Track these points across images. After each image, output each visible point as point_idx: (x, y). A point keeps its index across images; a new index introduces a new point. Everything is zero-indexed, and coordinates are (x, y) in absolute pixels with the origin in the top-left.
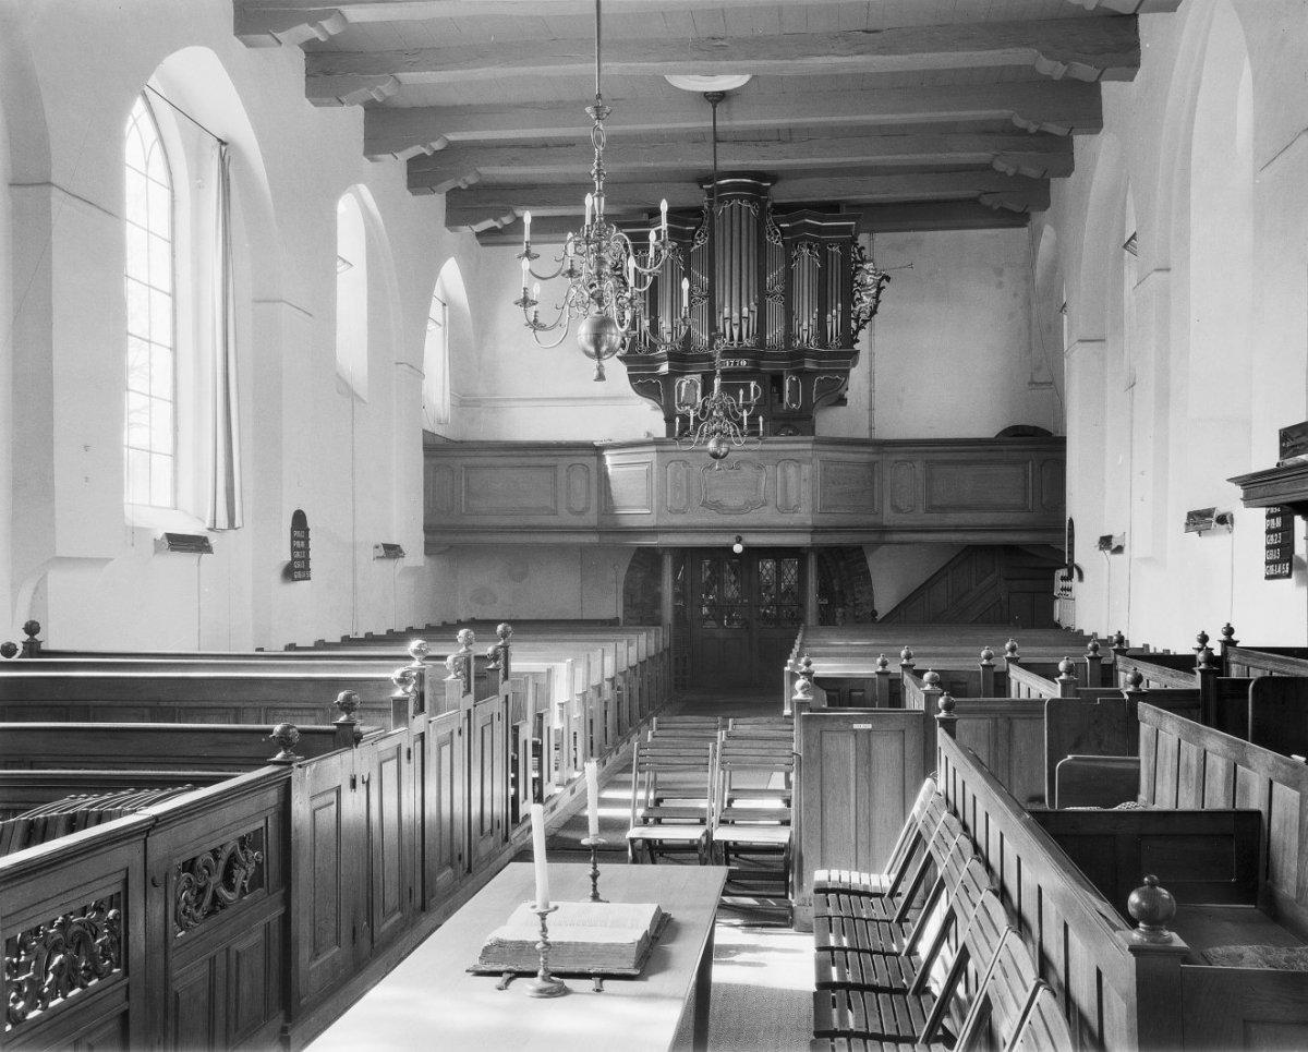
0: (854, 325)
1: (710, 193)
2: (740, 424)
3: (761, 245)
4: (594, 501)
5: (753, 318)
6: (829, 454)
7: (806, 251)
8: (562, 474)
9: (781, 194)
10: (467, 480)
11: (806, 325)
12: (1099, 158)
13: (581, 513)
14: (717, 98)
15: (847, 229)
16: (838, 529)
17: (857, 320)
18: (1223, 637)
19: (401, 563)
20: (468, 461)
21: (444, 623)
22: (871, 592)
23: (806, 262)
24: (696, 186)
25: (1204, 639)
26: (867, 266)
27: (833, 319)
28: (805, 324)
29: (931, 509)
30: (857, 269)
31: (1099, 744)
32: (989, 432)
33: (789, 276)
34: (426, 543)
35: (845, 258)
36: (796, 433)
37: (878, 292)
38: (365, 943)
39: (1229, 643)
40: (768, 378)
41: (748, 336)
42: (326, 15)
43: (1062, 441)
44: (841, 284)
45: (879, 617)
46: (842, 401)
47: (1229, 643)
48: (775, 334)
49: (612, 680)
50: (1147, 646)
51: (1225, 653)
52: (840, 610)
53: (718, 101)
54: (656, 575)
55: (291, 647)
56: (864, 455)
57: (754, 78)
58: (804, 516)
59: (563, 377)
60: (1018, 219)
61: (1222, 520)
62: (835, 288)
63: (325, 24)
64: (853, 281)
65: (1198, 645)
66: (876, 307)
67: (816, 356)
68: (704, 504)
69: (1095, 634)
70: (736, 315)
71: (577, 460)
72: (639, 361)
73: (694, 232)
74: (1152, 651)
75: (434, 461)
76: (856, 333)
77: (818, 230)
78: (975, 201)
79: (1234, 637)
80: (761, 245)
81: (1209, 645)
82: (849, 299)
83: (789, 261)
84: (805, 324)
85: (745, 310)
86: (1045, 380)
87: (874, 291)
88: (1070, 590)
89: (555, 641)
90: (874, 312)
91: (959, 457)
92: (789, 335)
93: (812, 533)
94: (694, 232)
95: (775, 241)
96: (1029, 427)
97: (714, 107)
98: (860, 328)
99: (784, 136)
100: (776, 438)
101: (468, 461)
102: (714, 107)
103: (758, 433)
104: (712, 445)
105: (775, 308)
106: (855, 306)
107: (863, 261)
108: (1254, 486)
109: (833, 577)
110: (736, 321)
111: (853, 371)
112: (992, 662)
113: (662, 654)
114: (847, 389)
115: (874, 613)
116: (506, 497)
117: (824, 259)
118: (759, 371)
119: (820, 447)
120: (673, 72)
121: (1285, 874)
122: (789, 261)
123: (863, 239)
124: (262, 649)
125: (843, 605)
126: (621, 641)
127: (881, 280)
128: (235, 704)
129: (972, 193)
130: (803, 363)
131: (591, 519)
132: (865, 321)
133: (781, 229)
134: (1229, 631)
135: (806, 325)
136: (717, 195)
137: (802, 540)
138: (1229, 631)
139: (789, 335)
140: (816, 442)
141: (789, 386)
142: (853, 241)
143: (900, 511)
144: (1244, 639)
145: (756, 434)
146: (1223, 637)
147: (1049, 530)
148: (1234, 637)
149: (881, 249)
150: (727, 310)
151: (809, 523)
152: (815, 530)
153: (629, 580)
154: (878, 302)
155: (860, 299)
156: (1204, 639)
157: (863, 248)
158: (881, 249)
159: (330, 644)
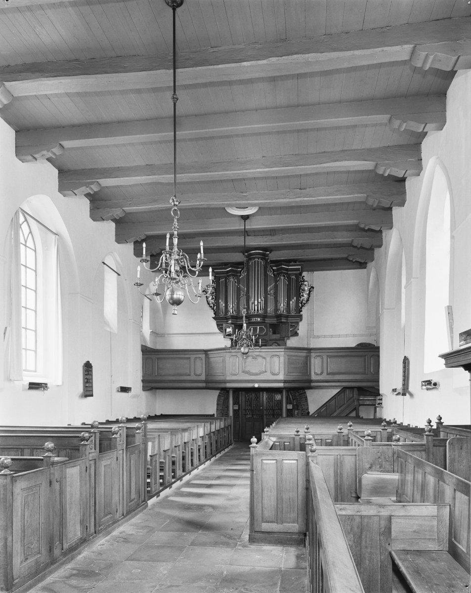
0: (300, 305)
1: (247, 257)
2: (252, 340)
3: (266, 275)
4: (204, 371)
5: (263, 303)
6: (288, 353)
7: (282, 278)
8: (192, 360)
9: (273, 256)
10: (158, 363)
11: (282, 306)
12: (392, 239)
13: (199, 375)
14: (245, 218)
15: (298, 269)
16: (293, 381)
17: (301, 303)
18: (437, 421)
19: (130, 394)
20: (158, 356)
21: (156, 415)
22: (308, 405)
23: (282, 282)
24: (241, 254)
25: (430, 422)
26: (306, 283)
27: (293, 302)
28: (282, 305)
29: (328, 374)
30: (302, 284)
31: (380, 467)
32: (354, 345)
33: (276, 287)
34: (143, 386)
35: (297, 280)
36: (279, 345)
37: (309, 293)
38: (57, 552)
39: (440, 423)
40: (268, 325)
41: (260, 309)
42: (92, 183)
43: (378, 348)
44: (296, 288)
45: (310, 414)
46: (296, 334)
47: (440, 423)
48: (270, 309)
49: (202, 437)
50: (409, 425)
51: (438, 427)
52: (296, 411)
53: (246, 219)
54: (228, 398)
55: (84, 424)
56: (304, 354)
57: (260, 208)
58: (281, 377)
59: (194, 328)
60: (362, 265)
61: (435, 384)
62: (293, 291)
63: (92, 186)
64: (300, 289)
65: (427, 424)
66: (309, 298)
67: (287, 317)
68: (243, 372)
69: (385, 419)
70: (256, 302)
71: (198, 356)
72: (221, 320)
73: (241, 271)
74: (411, 426)
75: (147, 356)
76: (301, 308)
77: (287, 270)
78: (347, 259)
79: (442, 421)
80: (266, 275)
81: (431, 424)
82: (299, 296)
83: (276, 281)
84: (282, 305)
85: (260, 300)
86: (375, 328)
87: (308, 292)
88: (381, 404)
89: (161, 422)
90: (308, 300)
91: (341, 354)
92: (276, 309)
93: (284, 382)
94: (241, 271)
95: (271, 274)
96: (367, 344)
97: (245, 222)
98: (302, 306)
99: (272, 232)
100: (271, 347)
101: (158, 356)
102: (245, 222)
103: (259, 345)
104: (242, 349)
105: (271, 298)
106: (301, 298)
107: (304, 281)
108: (450, 359)
109: (290, 400)
110: (256, 303)
111: (300, 324)
112: (342, 431)
113: (227, 427)
114: (298, 329)
115: (309, 413)
116: (169, 369)
117: (289, 279)
118: (264, 322)
119: (286, 350)
120: (231, 206)
121: (461, 538)
122: (276, 281)
123: (304, 274)
124: (70, 425)
125: (298, 409)
126: (208, 422)
127: (310, 288)
128: (21, 447)
129: (345, 256)
130: (281, 319)
131: (203, 378)
132: (304, 304)
133: (273, 269)
134: (440, 418)
135: (282, 306)
136: (250, 258)
137: (281, 385)
138: (440, 418)
139: (276, 309)
140: (285, 349)
141: (277, 328)
142: (301, 274)
143: (317, 375)
144: (446, 422)
145: (258, 346)
146: (437, 421)
147: (375, 382)
148: (442, 421)
149: (313, 278)
150: (253, 299)
151: (283, 379)
152: (285, 382)
153: (218, 400)
154: (309, 296)
155: (303, 296)
156: (430, 422)
157: (304, 276)
158: (313, 278)
159: (110, 421)
